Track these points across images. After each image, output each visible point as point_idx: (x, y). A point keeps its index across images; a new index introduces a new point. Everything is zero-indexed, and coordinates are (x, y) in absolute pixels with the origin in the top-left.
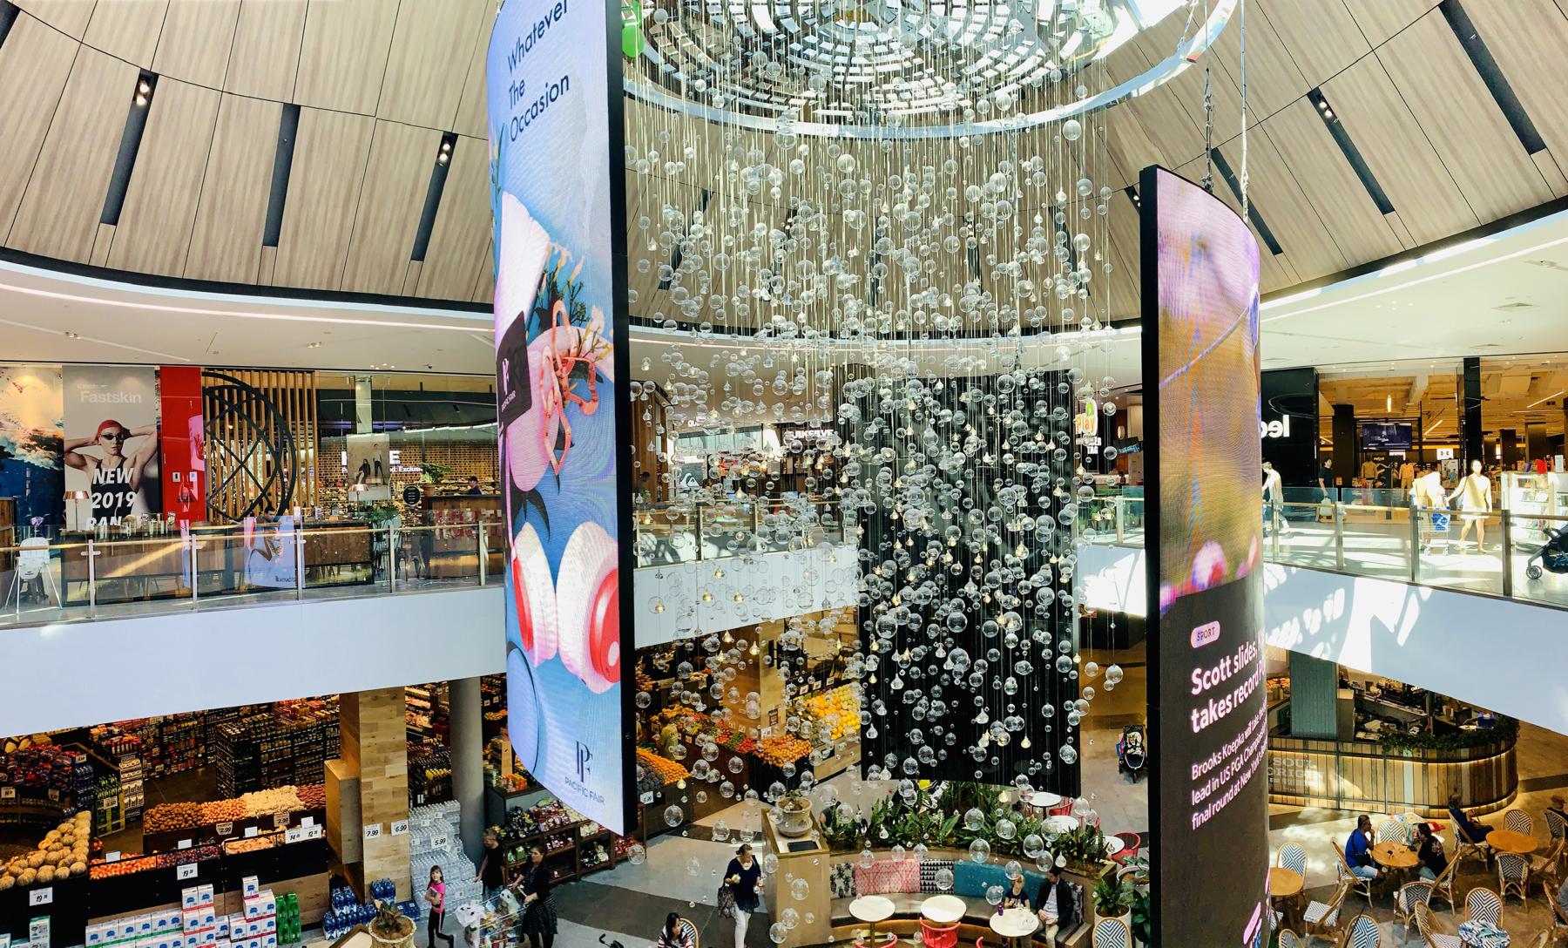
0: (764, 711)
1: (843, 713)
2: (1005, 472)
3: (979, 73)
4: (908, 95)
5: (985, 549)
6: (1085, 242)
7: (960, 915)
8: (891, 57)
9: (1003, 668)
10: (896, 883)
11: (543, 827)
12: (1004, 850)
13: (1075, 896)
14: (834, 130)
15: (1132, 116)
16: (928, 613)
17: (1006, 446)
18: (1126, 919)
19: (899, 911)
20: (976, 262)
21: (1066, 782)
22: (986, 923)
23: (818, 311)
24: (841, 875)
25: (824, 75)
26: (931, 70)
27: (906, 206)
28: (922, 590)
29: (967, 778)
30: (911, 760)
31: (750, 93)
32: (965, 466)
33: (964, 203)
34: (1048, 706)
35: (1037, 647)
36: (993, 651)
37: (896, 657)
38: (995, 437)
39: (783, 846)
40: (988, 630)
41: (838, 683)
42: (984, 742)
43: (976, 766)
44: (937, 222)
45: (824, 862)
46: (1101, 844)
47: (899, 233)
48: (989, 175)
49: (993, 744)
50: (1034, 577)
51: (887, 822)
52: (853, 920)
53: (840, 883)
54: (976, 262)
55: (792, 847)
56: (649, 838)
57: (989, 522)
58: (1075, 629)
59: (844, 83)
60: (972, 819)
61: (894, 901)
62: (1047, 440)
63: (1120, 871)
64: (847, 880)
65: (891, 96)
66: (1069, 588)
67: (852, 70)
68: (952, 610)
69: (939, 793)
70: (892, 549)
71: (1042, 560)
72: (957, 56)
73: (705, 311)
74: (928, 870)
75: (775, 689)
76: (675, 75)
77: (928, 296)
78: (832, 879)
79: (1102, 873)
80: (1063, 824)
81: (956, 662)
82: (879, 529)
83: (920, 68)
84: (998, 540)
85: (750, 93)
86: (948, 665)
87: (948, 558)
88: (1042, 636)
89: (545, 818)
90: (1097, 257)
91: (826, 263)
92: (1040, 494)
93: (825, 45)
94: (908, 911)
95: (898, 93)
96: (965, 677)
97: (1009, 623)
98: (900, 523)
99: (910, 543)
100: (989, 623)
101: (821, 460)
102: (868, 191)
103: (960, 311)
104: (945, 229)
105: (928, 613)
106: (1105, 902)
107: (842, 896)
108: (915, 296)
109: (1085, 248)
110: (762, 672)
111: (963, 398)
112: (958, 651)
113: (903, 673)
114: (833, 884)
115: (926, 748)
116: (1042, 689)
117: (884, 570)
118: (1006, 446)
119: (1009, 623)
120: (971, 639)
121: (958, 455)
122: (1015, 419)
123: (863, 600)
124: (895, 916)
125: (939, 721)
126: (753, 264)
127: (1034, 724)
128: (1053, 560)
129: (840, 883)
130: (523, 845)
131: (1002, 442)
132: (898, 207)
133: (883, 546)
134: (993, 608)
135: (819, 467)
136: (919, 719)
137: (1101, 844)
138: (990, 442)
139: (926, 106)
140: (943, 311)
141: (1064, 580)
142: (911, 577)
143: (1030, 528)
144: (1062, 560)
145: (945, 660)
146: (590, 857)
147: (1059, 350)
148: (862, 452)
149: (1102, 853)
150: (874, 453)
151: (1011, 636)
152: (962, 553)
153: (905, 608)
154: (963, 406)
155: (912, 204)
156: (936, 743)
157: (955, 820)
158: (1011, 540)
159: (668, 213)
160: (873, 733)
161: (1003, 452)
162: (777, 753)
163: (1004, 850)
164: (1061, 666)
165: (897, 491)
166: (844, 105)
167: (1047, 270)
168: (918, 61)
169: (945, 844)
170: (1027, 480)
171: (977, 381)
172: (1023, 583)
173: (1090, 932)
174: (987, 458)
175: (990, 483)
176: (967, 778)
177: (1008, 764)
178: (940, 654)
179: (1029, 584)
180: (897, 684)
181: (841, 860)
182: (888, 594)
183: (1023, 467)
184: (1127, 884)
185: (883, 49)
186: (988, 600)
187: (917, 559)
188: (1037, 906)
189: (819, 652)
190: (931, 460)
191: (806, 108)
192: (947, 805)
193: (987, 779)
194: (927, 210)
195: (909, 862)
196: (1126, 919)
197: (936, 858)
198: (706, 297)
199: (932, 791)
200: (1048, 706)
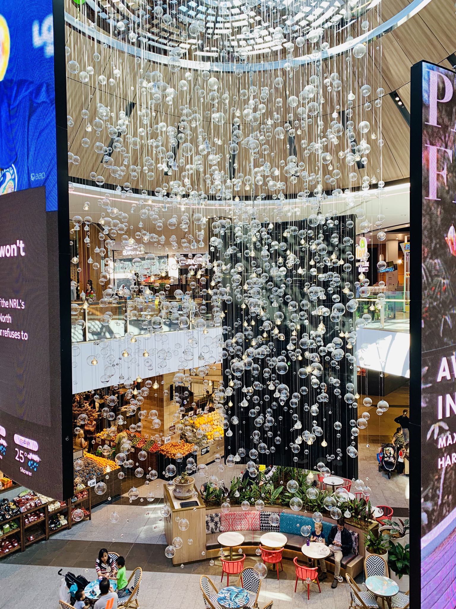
0: (168, 426)
1: (213, 425)
2: (312, 279)
3: (297, 23)
4: (252, 42)
5: (299, 327)
6: (366, 126)
7: (284, 544)
8: (242, 17)
9: (311, 397)
10: (244, 525)
11: (23, 509)
12: (309, 506)
13: (353, 539)
14: (207, 66)
15: (396, 44)
16: (264, 364)
17: (312, 263)
18: (385, 557)
19: (247, 541)
20: (293, 146)
21: (348, 469)
22: (300, 550)
23: (197, 180)
24: (212, 520)
25: (198, 25)
26: (266, 24)
27: (251, 111)
28: (260, 350)
29: (286, 460)
30: (253, 451)
31: (156, 38)
32: (286, 276)
33: (287, 109)
34: (337, 423)
35: (330, 388)
36: (304, 388)
37: (245, 390)
38: (304, 257)
39: (177, 505)
40: (301, 374)
41: (211, 410)
42: (299, 441)
43: (295, 455)
44: (270, 122)
45: (203, 513)
46: (369, 510)
47: (247, 128)
48: (304, 86)
49: (304, 445)
50: (329, 345)
51: (240, 490)
52: (220, 546)
53: (212, 525)
54: (293, 146)
55: (182, 505)
56: (93, 507)
57: (301, 310)
58: (354, 377)
59: (213, 34)
60: (291, 487)
61: (244, 535)
62: (339, 258)
63: (380, 528)
64: (216, 523)
65: (242, 43)
66: (351, 351)
67: (218, 25)
68: (278, 362)
69: (271, 474)
70: (241, 326)
71: (336, 334)
72: (283, 12)
73: (127, 178)
74: (264, 517)
75: (173, 412)
76: (108, 20)
77: (265, 169)
78: (207, 523)
79: (370, 528)
80: (346, 496)
81: (282, 393)
82: (234, 314)
83: (259, 23)
84: (306, 322)
85: (156, 38)
86: (277, 395)
87: (276, 331)
88: (334, 380)
89: (24, 504)
90: (373, 137)
91: (201, 147)
92: (334, 293)
93: (200, 8)
94: (252, 541)
95: (246, 40)
96: (287, 403)
97: (313, 371)
98: (247, 310)
99: (253, 323)
100: (302, 370)
101: (200, 273)
102: (227, 101)
103: (284, 179)
104: (275, 125)
105: (264, 364)
106: (372, 544)
107: (213, 532)
108: (256, 169)
109: (366, 131)
110: (165, 403)
111: (285, 234)
112: (283, 386)
113: (248, 398)
114: (207, 525)
115: (263, 445)
116: (334, 413)
117: (239, 337)
118: (312, 263)
119: (313, 371)
120: (290, 379)
121: (283, 269)
122: (318, 244)
123: (225, 355)
124: (244, 544)
125: (271, 429)
126: (157, 147)
127: (329, 433)
128: (342, 335)
129: (212, 525)
130: (9, 523)
131: (310, 260)
132: (246, 112)
133: (236, 324)
134: (305, 362)
135: (199, 276)
136: (258, 426)
137: (369, 510)
138: (302, 259)
139: (264, 48)
140: (274, 178)
141: (349, 346)
142: (254, 343)
143: (327, 314)
144: (347, 335)
145: (274, 391)
146: (55, 523)
147: (344, 202)
148: (224, 267)
149: (370, 515)
150: (231, 268)
151: (314, 380)
152: (285, 330)
153: (250, 359)
154: (285, 240)
155: (255, 110)
156: (270, 442)
157: (281, 489)
158: (315, 321)
159: (103, 110)
160: (230, 433)
161: (311, 267)
162: (173, 451)
163: (309, 506)
164: (348, 399)
165: (246, 292)
166: (213, 49)
167: (341, 147)
168: (258, 18)
169: (275, 503)
170: (326, 285)
171: (296, 223)
172: (322, 348)
173: (362, 561)
174: (300, 271)
175: (302, 286)
176: (286, 460)
177: (312, 457)
178: (271, 387)
179: (326, 349)
180: (245, 403)
181: (213, 512)
182: (239, 353)
183: (322, 277)
184: (385, 536)
185: (237, 11)
186: (300, 358)
187: (257, 332)
188: (329, 542)
189: (199, 392)
190: (264, 271)
191: (190, 50)
192: (276, 481)
193: (301, 466)
194: (264, 114)
195: (252, 513)
196: (385, 557)
197: (269, 510)
198: (127, 167)
199: (266, 473)
200: (337, 423)
